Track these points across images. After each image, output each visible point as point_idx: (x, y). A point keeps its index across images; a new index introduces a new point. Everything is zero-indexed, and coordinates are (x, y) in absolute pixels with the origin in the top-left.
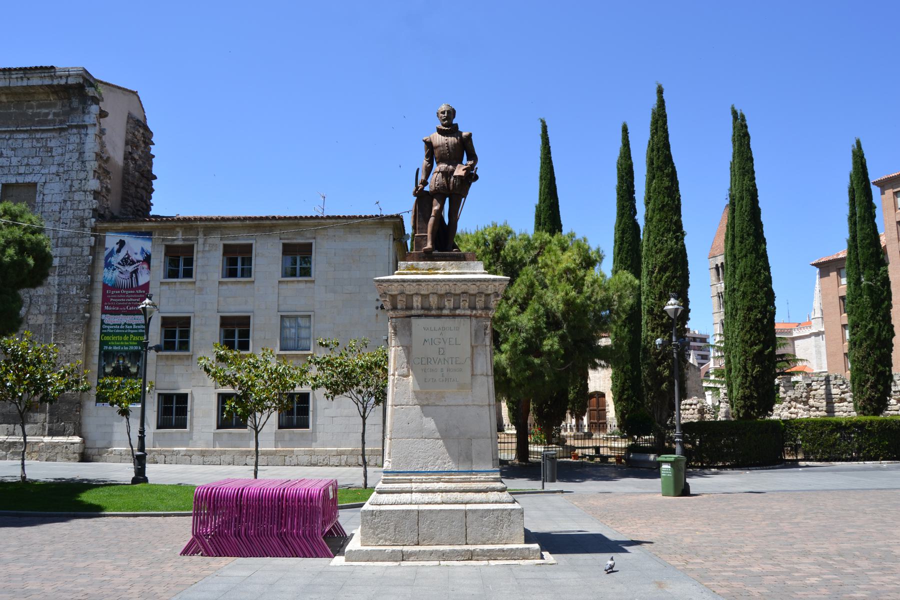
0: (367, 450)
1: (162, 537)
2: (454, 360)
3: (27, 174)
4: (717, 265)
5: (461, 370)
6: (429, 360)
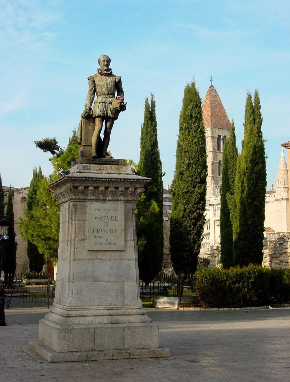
0: (6, 315)
1: (47, 303)
2: (114, 231)
4: (219, 136)
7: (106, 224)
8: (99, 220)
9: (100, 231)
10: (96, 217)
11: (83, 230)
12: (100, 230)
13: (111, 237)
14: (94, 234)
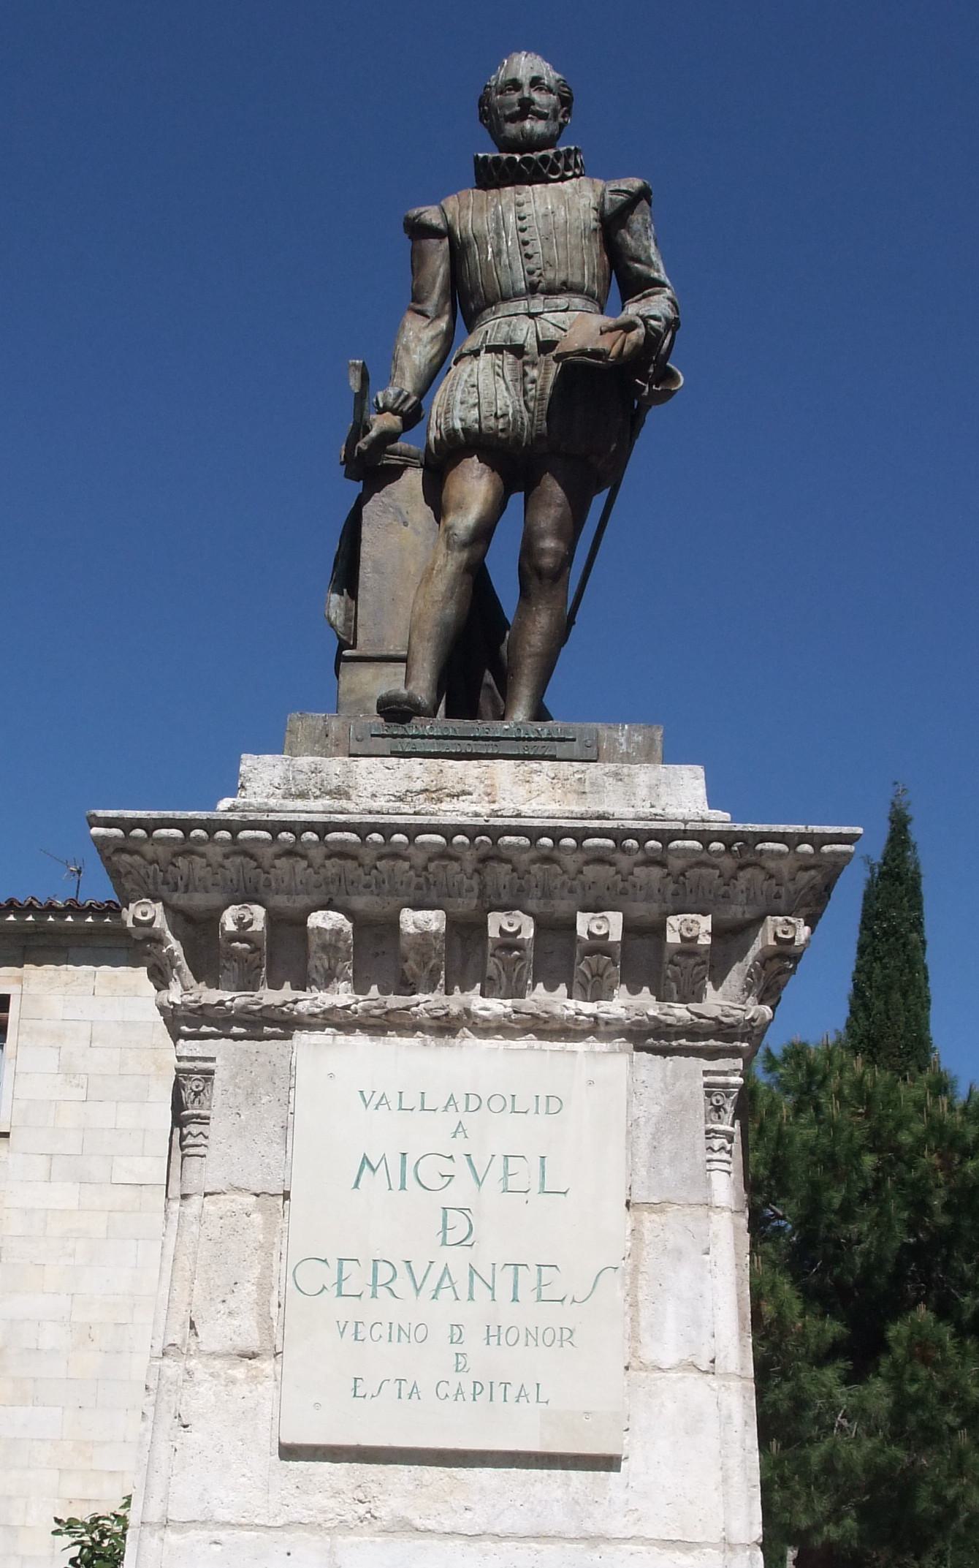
2: (528, 1279)
3: (634, 1285)
5: (566, 1336)
6: (385, 1273)
7: (454, 1217)
8: (396, 1183)
9: (403, 1284)
10: (365, 1160)
11: (256, 1271)
12: (402, 1269)
13: (493, 1334)
14: (345, 1310)
